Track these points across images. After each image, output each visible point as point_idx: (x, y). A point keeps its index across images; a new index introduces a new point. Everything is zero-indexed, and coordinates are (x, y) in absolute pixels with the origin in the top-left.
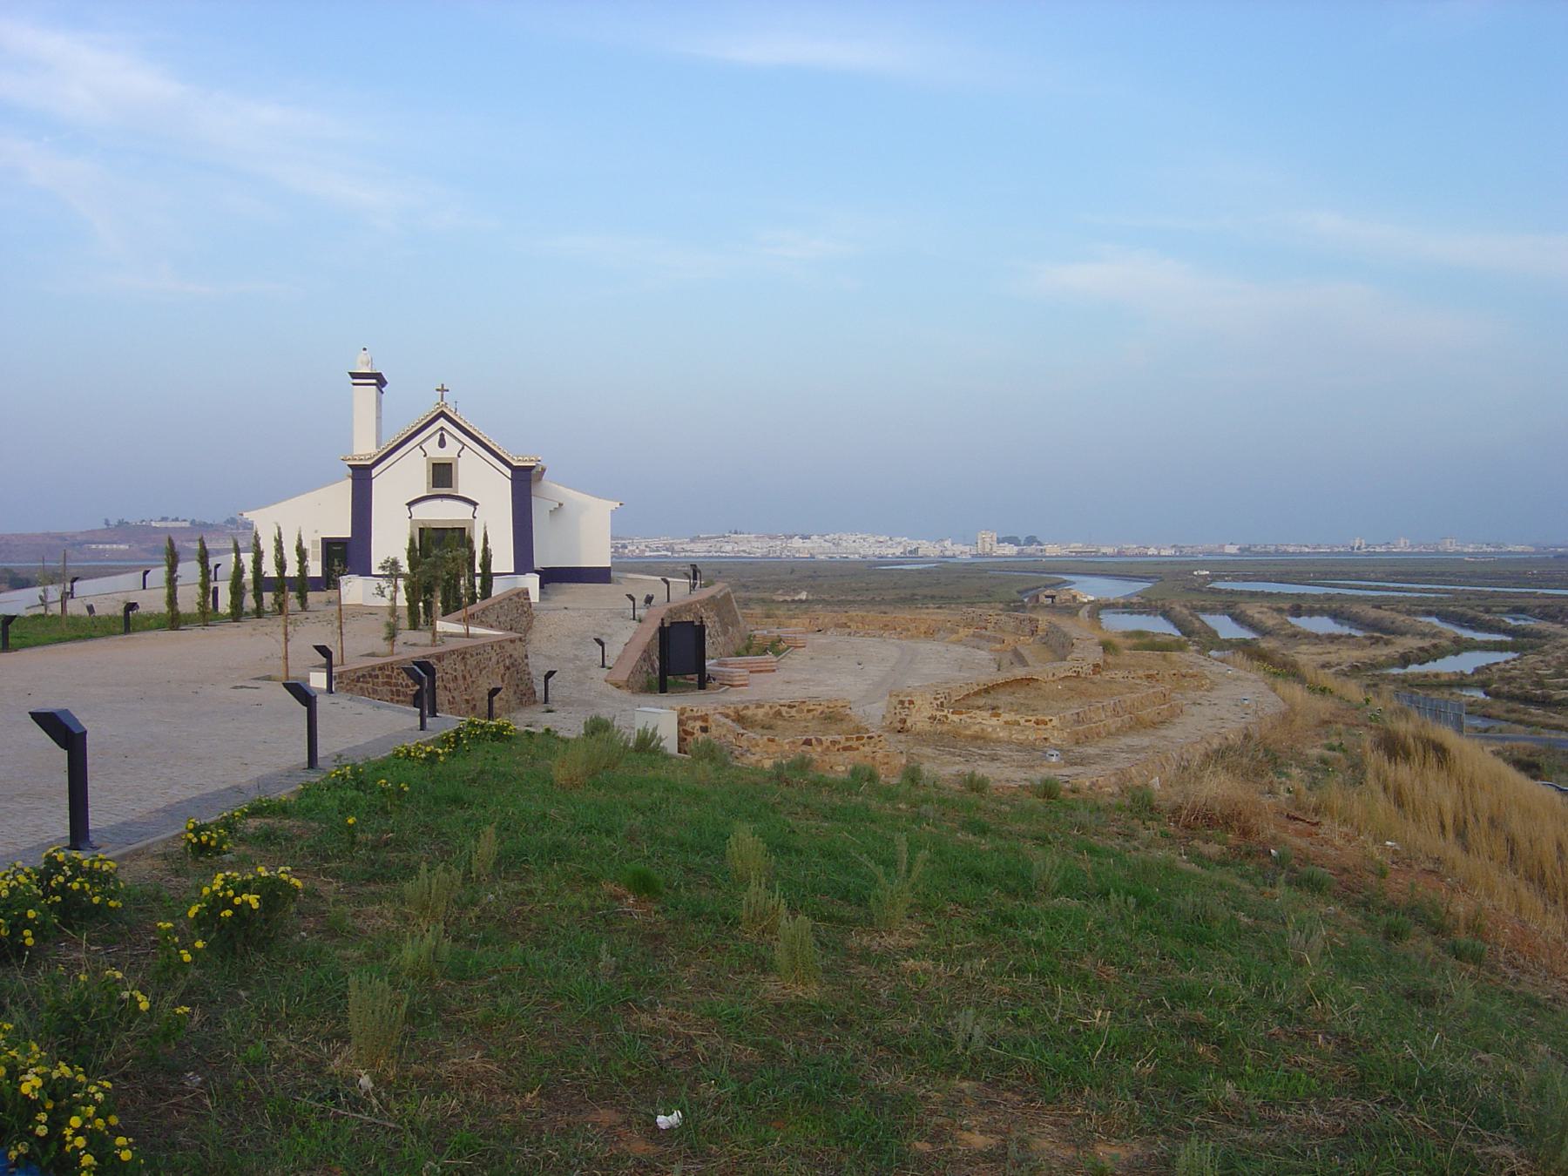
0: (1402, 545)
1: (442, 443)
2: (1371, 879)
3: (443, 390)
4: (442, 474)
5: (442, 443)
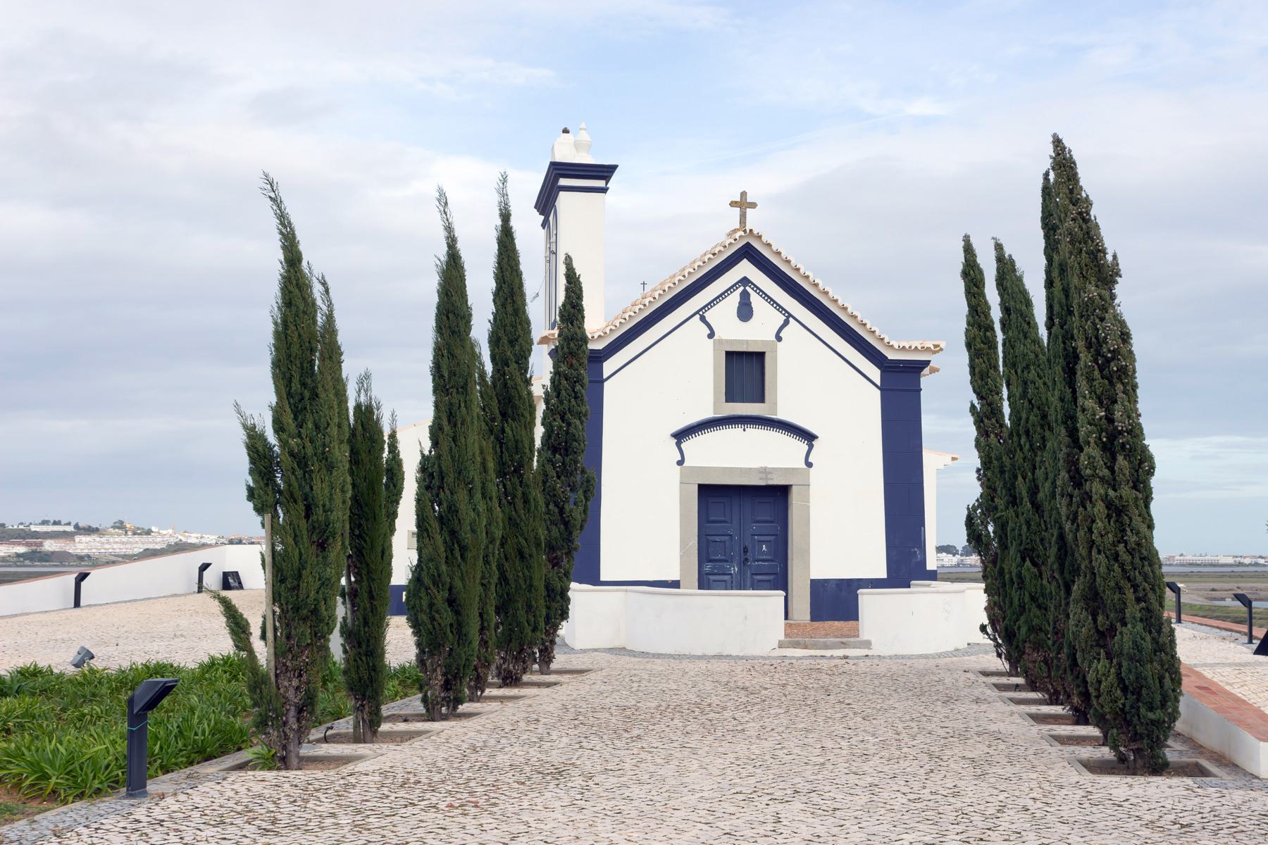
0: (1189, 558)
1: (745, 312)
2: (989, 630)
3: (743, 204)
4: (745, 372)
5: (745, 312)
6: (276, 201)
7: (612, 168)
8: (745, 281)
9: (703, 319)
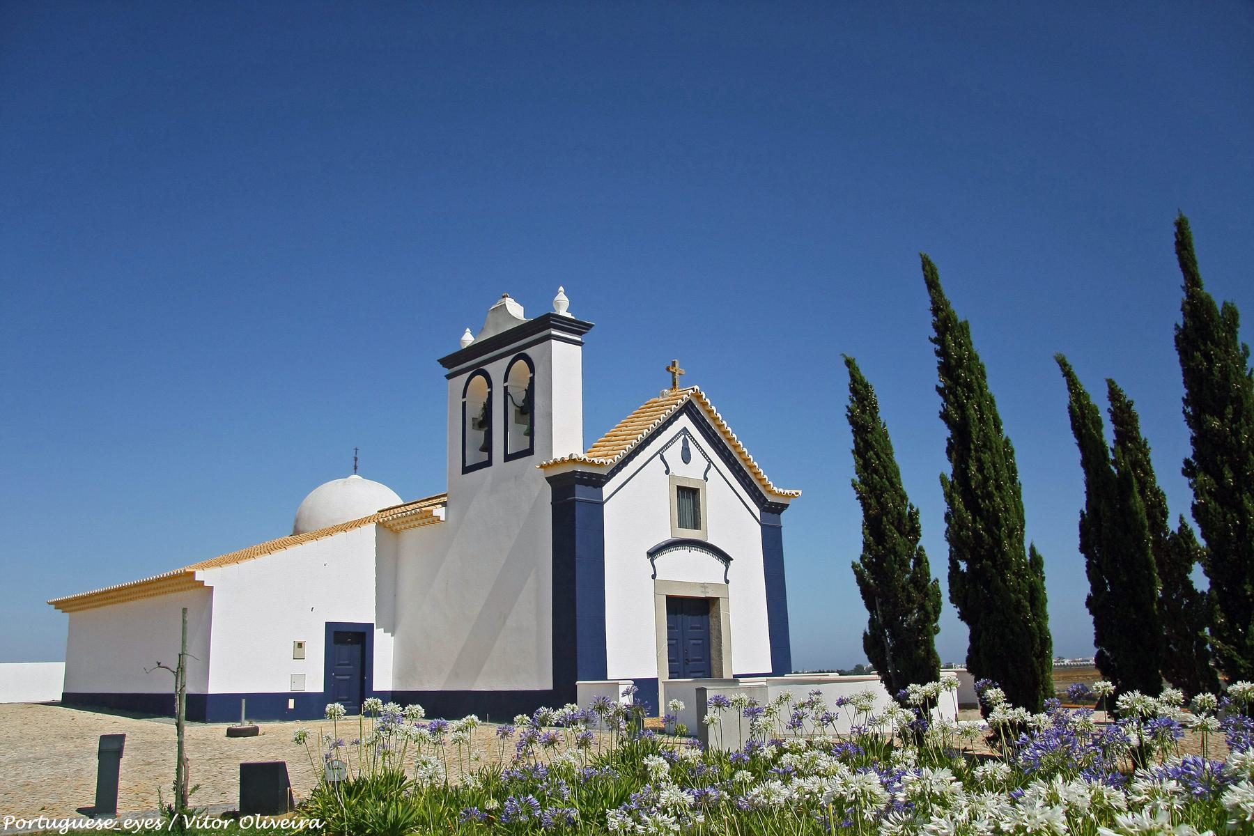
1: (686, 457)
5: (686, 457)
6: (1068, 374)
7: (590, 326)
8: (685, 431)
9: (662, 458)
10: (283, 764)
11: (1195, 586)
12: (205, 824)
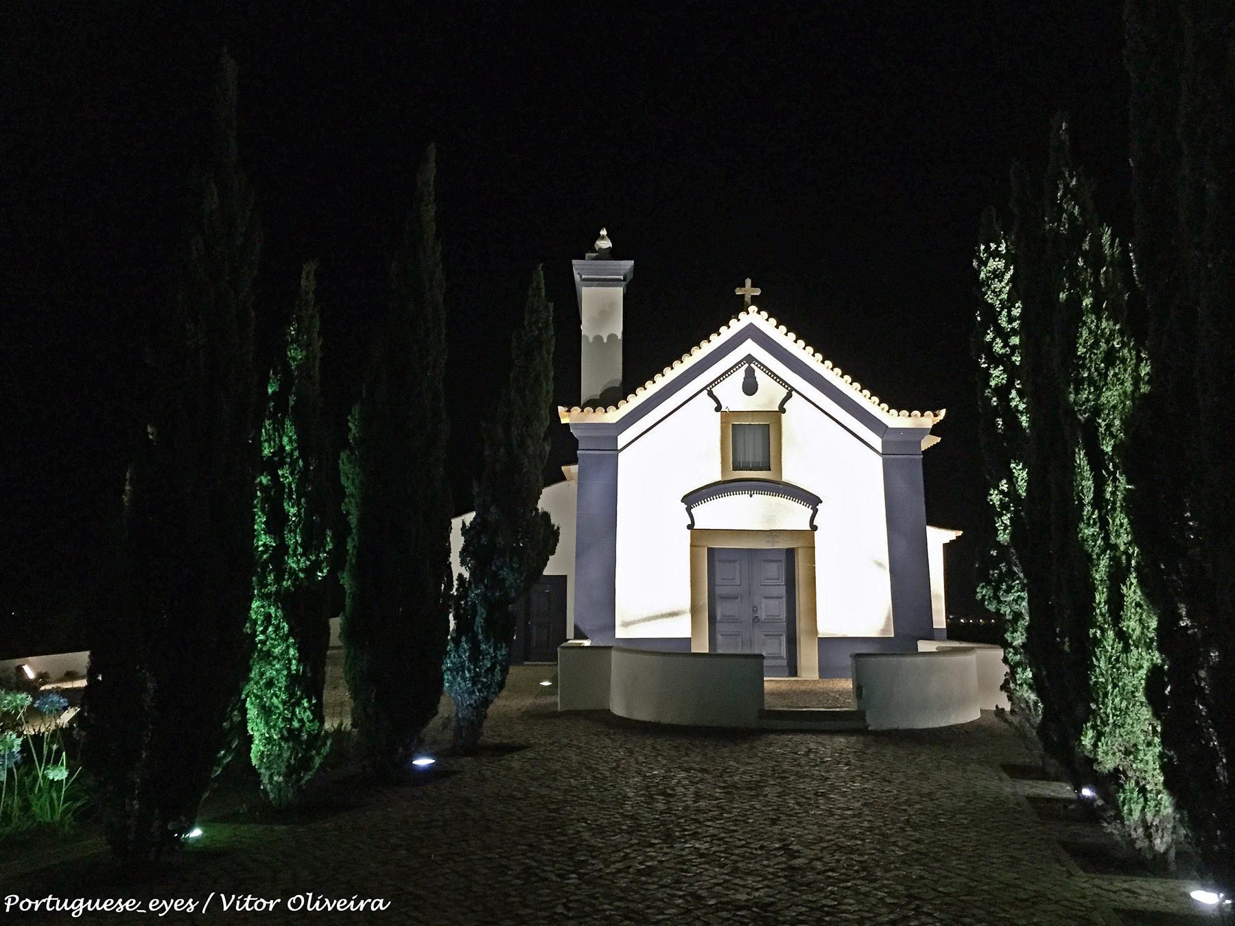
9: (711, 394)
10: (945, 545)
11: (874, 632)
12: (247, 905)
